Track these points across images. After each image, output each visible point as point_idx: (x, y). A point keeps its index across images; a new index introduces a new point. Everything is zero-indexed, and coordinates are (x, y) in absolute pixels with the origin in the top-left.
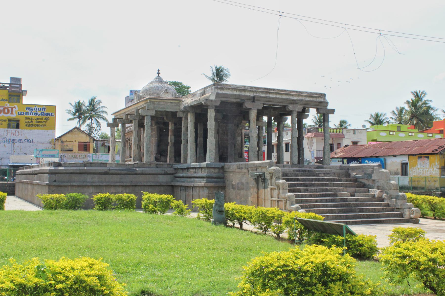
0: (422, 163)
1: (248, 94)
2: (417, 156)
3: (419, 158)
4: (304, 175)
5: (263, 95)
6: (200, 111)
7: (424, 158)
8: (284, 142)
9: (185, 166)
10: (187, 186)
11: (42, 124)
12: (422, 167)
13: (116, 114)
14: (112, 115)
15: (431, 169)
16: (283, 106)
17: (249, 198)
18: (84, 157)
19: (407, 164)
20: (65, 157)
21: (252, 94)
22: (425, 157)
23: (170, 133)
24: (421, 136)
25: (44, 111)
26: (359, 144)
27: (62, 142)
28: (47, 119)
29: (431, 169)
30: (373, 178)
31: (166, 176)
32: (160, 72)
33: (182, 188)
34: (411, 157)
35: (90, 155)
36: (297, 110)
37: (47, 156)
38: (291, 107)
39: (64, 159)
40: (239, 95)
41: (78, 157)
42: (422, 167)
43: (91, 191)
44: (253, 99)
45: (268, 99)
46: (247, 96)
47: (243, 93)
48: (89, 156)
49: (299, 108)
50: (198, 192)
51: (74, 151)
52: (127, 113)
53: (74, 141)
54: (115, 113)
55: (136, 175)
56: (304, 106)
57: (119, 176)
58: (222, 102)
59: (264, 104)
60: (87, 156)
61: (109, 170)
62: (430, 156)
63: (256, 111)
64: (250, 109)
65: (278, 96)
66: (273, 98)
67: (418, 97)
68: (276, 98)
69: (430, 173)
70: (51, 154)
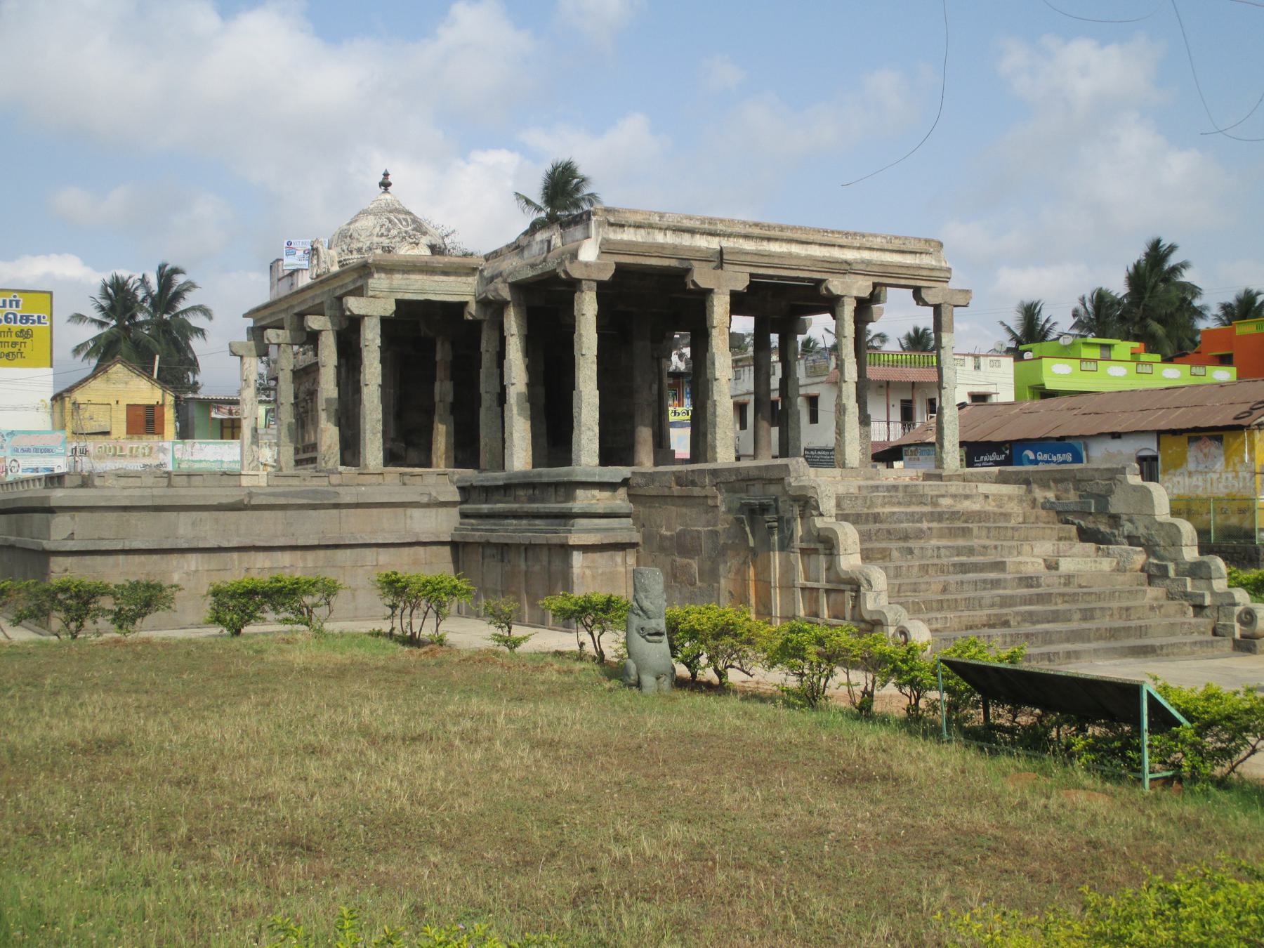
0: (1201, 456)
1: (702, 242)
2: (1185, 436)
3: (1190, 440)
4: (893, 504)
5: (749, 246)
6: (546, 300)
7: (1208, 442)
8: (802, 391)
9: (496, 477)
10: (507, 544)
11: (11, 349)
12: (1201, 468)
13: (260, 315)
14: (245, 316)
15: (1230, 475)
16: (810, 280)
17: (722, 581)
18: (147, 451)
19: (1155, 459)
20: (85, 452)
21: (714, 243)
22: (1211, 438)
23: (440, 373)
24: (1174, 374)
25: (14, 309)
26: (994, 399)
27: (76, 406)
28: (26, 334)
29: (1230, 475)
30: (1113, 510)
31: (433, 511)
32: (390, 179)
33: (488, 552)
34: (1167, 440)
35: (167, 445)
36: (855, 293)
37: (29, 450)
38: (836, 285)
39: (84, 459)
40: (675, 247)
41: (127, 452)
42: (1201, 468)
43: (193, 568)
44: (720, 259)
45: (766, 260)
46: (699, 250)
47: (686, 240)
48: (164, 450)
49: (862, 287)
50: (545, 563)
51: (114, 435)
52: (296, 310)
53: (113, 403)
54: (258, 310)
55: (335, 511)
56: (877, 280)
57: (280, 514)
58: (620, 268)
59: (752, 275)
60: (155, 448)
61: (250, 495)
62: (1225, 434)
63: (728, 298)
64: (710, 291)
65: (795, 249)
66: (780, 256)
67: (1157, 254)
68: (790, 254)
69: (1226, 487)
70: (40, 445)
